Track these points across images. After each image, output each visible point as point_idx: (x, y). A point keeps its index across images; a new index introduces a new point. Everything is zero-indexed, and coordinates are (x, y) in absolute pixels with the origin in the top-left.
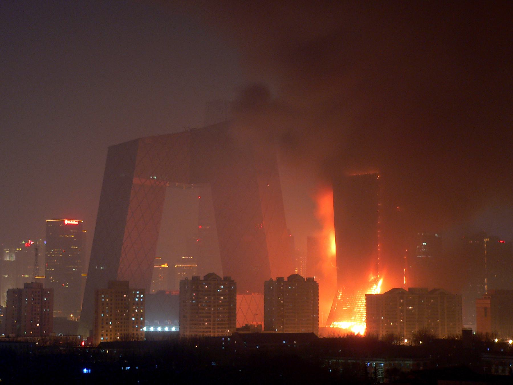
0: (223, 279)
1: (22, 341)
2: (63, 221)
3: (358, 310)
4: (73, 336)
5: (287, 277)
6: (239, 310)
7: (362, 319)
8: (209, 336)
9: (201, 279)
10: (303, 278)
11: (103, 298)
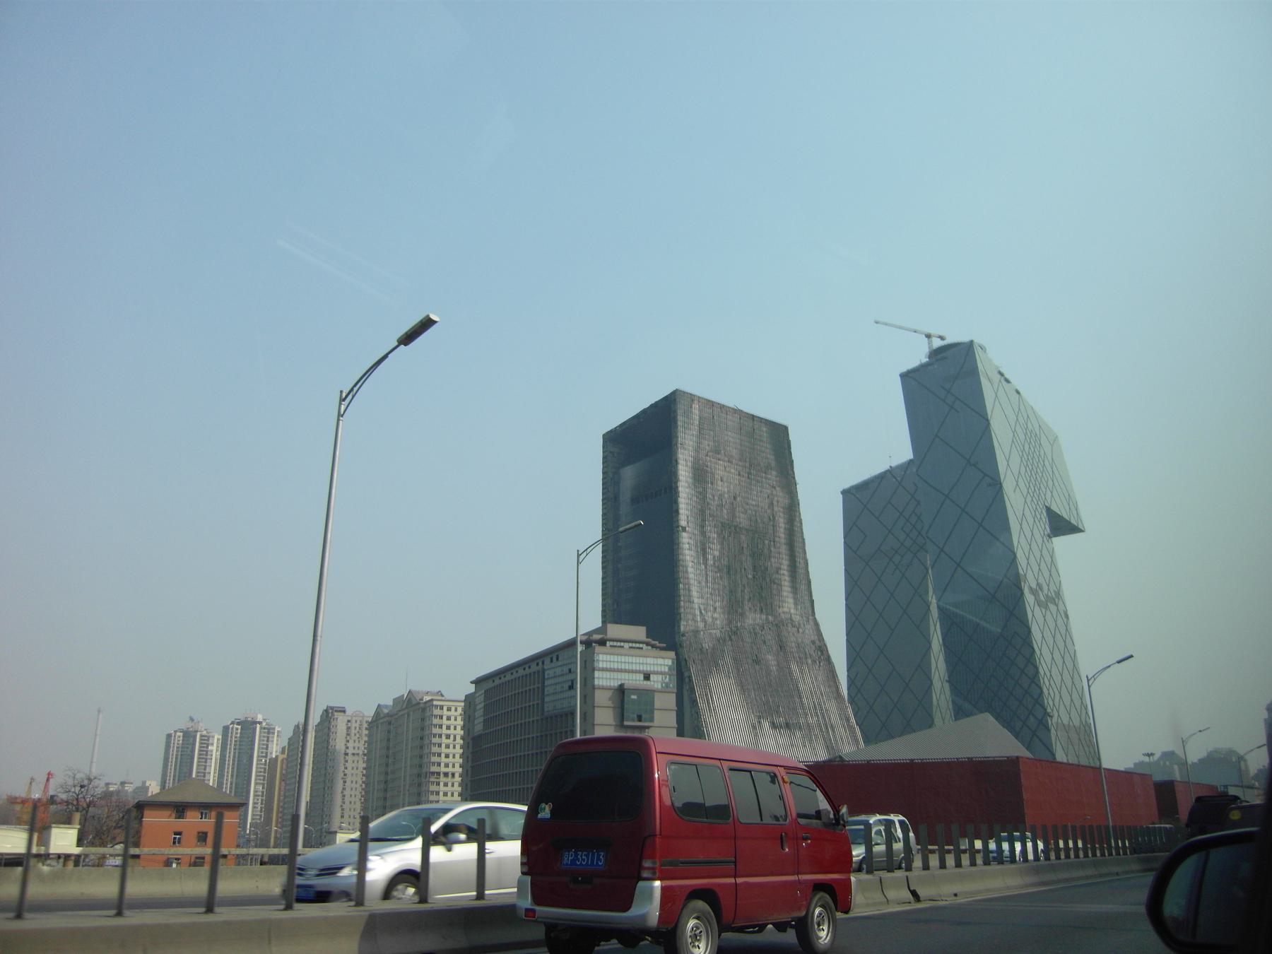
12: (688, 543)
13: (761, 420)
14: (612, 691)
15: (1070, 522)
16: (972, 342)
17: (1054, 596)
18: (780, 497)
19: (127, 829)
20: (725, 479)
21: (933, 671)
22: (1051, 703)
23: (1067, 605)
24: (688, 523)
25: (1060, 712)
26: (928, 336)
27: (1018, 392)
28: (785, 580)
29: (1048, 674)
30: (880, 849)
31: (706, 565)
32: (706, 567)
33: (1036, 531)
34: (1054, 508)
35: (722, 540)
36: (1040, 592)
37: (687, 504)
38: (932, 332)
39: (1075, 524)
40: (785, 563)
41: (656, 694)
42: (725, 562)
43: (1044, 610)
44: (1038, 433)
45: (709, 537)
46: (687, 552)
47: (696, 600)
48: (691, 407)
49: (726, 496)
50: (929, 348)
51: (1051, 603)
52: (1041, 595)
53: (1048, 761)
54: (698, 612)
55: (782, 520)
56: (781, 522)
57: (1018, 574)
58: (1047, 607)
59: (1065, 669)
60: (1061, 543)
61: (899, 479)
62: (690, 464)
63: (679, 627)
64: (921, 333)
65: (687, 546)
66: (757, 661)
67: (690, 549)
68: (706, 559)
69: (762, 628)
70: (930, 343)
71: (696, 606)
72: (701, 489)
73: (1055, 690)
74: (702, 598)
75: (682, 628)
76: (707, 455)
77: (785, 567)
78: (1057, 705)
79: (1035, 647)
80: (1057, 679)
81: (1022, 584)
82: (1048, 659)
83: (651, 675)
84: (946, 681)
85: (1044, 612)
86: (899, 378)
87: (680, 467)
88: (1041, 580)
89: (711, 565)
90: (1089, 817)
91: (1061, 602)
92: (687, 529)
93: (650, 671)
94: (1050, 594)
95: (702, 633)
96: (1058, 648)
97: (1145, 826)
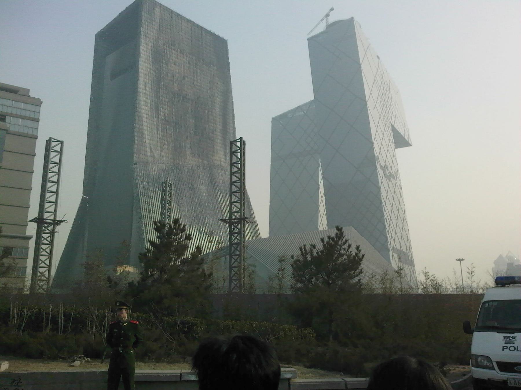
0: (28, 293)
1: (166, 363)
2: (470, 364)
3: (183, 216)
4: (426, 276)
5: (30, 91)
6: (367, 50)
7: (214, 121)
8: (46, 362)
9: (416, 367)
10: (194, 380)
11: (172, 253)
12: (145, 101)
14: (18, 93)
15: (404, 138)
16: (352, 19)
17: (394, 175)
19: (241, 193)
21: (391, 258)
22: (390, 235)
23: (402, 182)
24: (145, 87)
25: (393, 242)
27: (378, 57)
28: (218, 139)
29: (389, 218)
30: (203, 254)
31: (158, 118)
32: (158, 121)
33: (385, 135)
34: (396, 126)
36: (386, 170)
37: (146, 74)
39: (407, 139)
40: (219, 128)
41: (5, 152)
43: (388, 181)
44: (389, 84)
45: (162, 100)
48: (154, 9)
49: (177, 75)
50: (326, 23)
51: (393, 178)
52: (387, 172)
53: (35, 121)
54: (148, 150)
55: (218, 100)
56: (218, 100)
57: (374, 156)
58: (390, 180)
59: (396, 237)
60: (400, 152)
61: (305, 112)
63: (133, 158)
66: (192, 189)
68: (158, 114)
69: (198, 167)
73: (393, 227)
75: (135, 159)
76: (164, 45)
77: (219, 131)
78: (393, 236)
79: (383, 200)
80: (394, 222)
81: (377, 162)
82: (390, 208)
83: (7, 116)
84: (264, 293)
85: (401, 249)
86: (307, 41)
87: (142, 47)
88: (387, 163)
89: (162, 120)
90: (351, 264)
91: (398, 180)
93: (7, 113)
94: (392, 172)
95: (151, 164)
96: (395, 202)
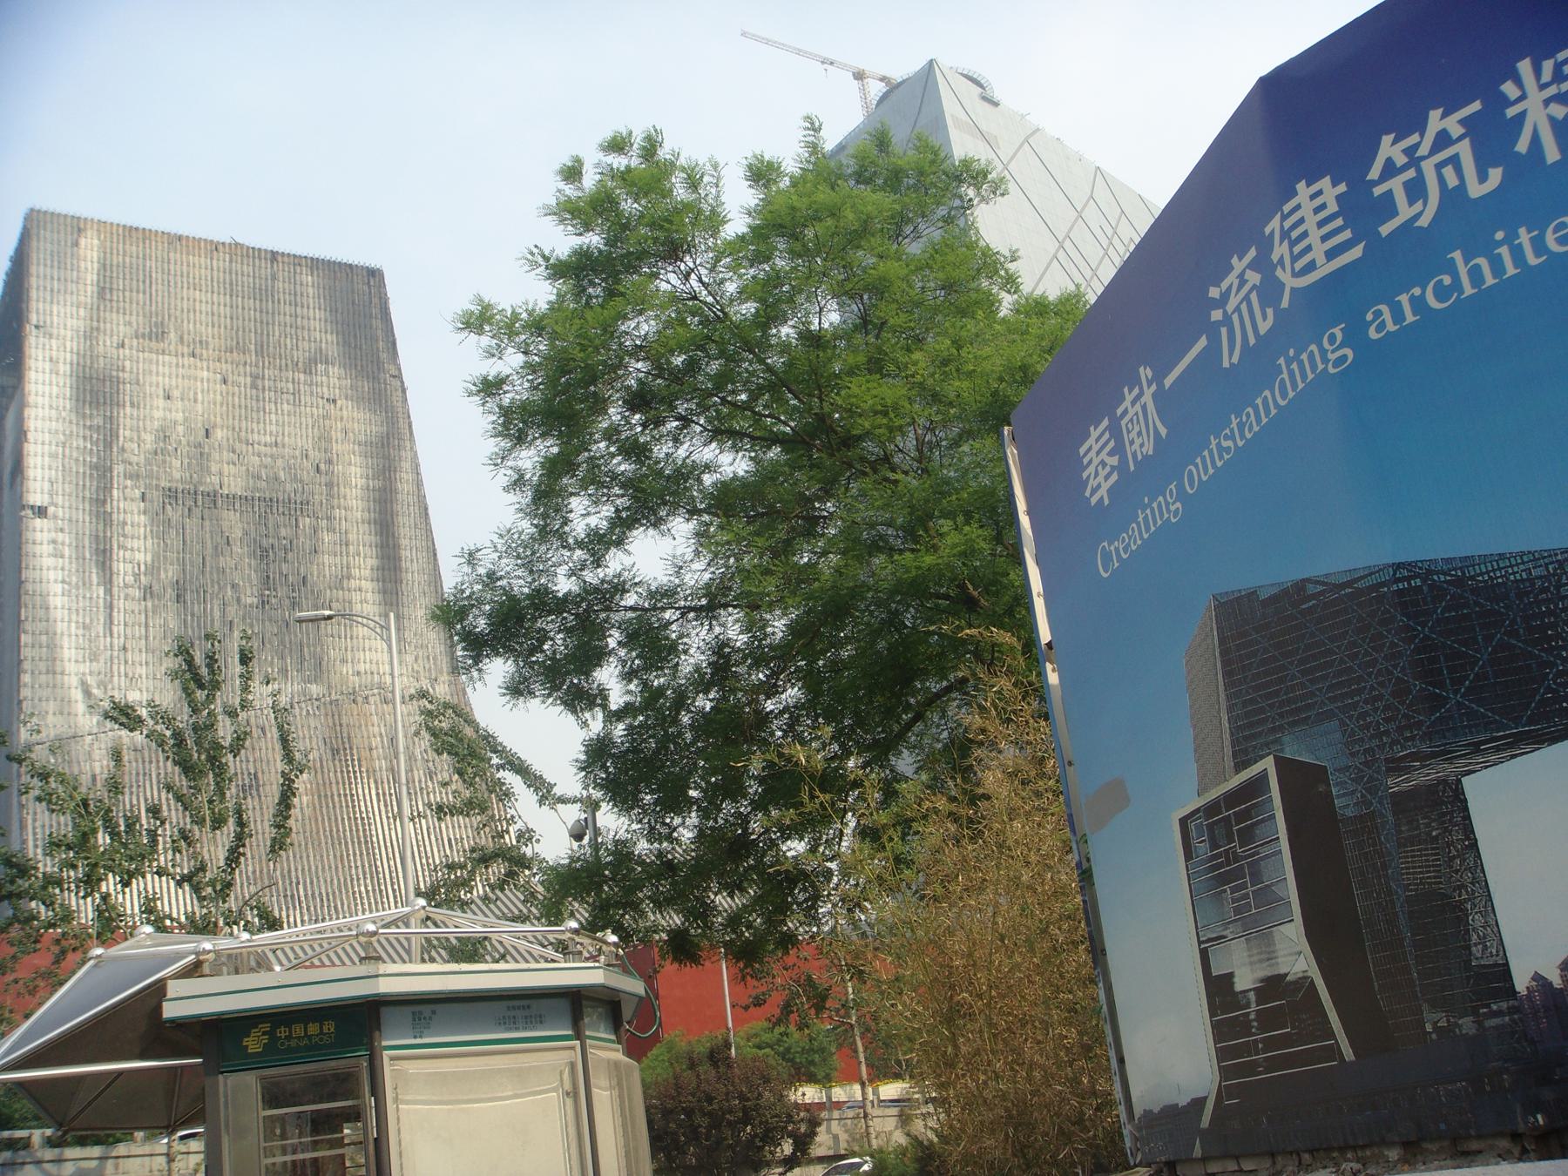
13: (297, 260)
18: (356, 420)
20: (176, 393)
26: (859, 76)
31: (108, 580)
32: (109, 591)
35: (160, 525)
38: (867, 67)
40: (364, 565)
42: (170, 573)
46: (48, 562)
47: (71, 667)
48: (76, 244)
54: (77, 695)
62: (64, 368)
64: (843, 67)
65: (58, 588)
67: (58, 555)
70: (863, 90)
71: (74, 681)
72: (98, 421)
74: (94, 658)
92: (51, 510)
97: (924, 777)
